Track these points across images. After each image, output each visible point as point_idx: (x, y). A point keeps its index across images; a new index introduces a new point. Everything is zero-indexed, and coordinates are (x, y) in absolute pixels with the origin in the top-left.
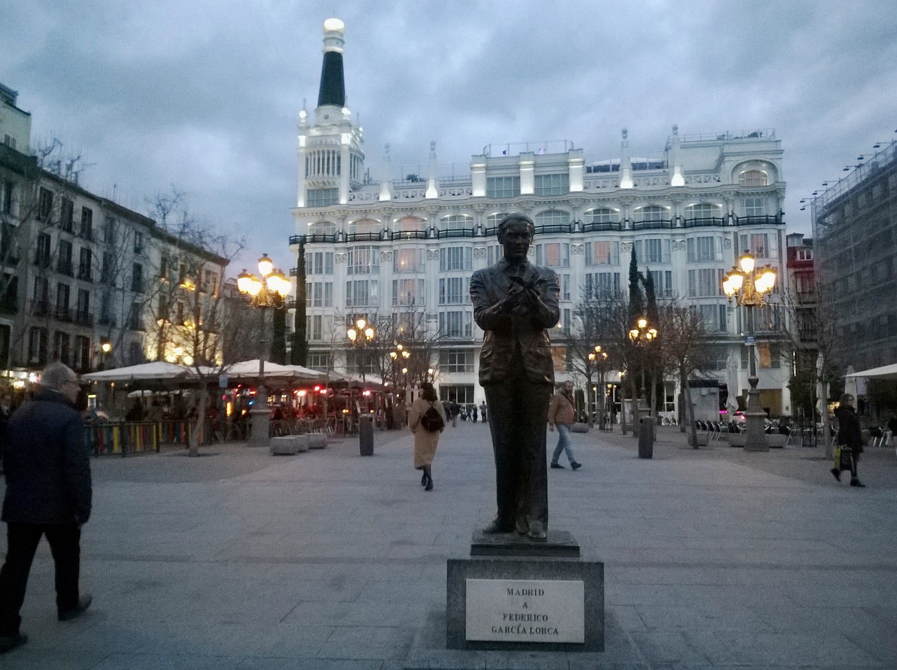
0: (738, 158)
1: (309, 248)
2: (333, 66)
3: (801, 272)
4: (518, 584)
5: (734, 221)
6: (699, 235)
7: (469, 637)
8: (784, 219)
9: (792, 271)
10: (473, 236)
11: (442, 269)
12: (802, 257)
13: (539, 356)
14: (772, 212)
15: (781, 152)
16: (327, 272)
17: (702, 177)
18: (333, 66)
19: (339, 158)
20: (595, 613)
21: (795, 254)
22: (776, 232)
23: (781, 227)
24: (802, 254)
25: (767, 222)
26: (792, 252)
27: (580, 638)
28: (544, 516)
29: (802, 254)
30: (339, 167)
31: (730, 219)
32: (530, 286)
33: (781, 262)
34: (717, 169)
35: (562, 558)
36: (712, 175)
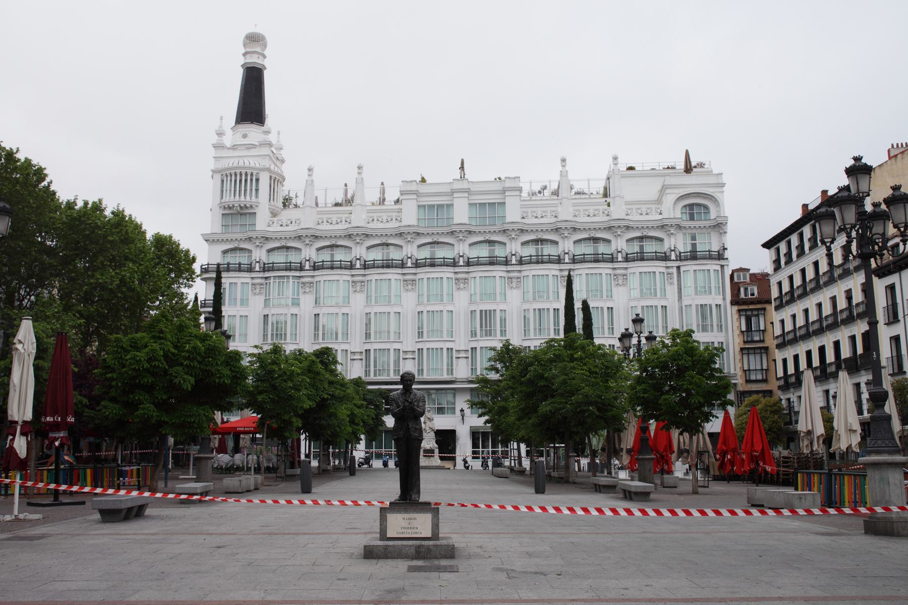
0: (676, 191)
1: (226, 280)
2: (253, 79)
3: (746, 310)
4: (406, 516)
5: (676, 256)
6: (534, 273)
7: (388, 536)
8: (727, 254)
9: (736, 308)
10: (402, 267)
11: (524, 301)
12: (746, 295)
13: (416, 429)
14: (715, 247)
15: (723, 185)
16: (242, 304)
17: (644, 208)
18: (253, 79)
19: (257, 180)
20: (436, 526)
21: (739, 290)
22: (718, 268)
23: (722, 262)
24: (746, 289)
25: (710, 257)
26: (735, 287)
27: (430, 536)
28: (419, 492)
29: (746, 289)
30: (257, 190)
31: (673, 253)
32: (411, 403)
33: (724, 299)
34: (659, 201)
35: (426, 507)
36: (653, 207)
